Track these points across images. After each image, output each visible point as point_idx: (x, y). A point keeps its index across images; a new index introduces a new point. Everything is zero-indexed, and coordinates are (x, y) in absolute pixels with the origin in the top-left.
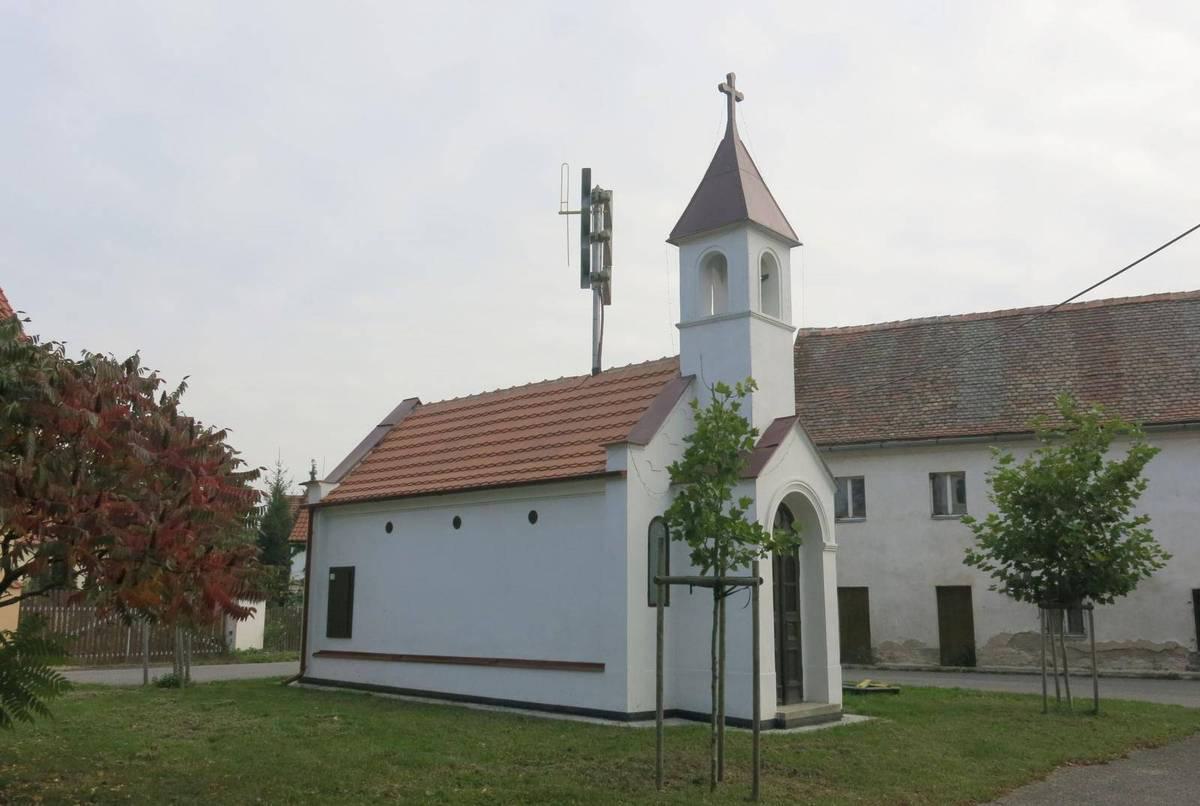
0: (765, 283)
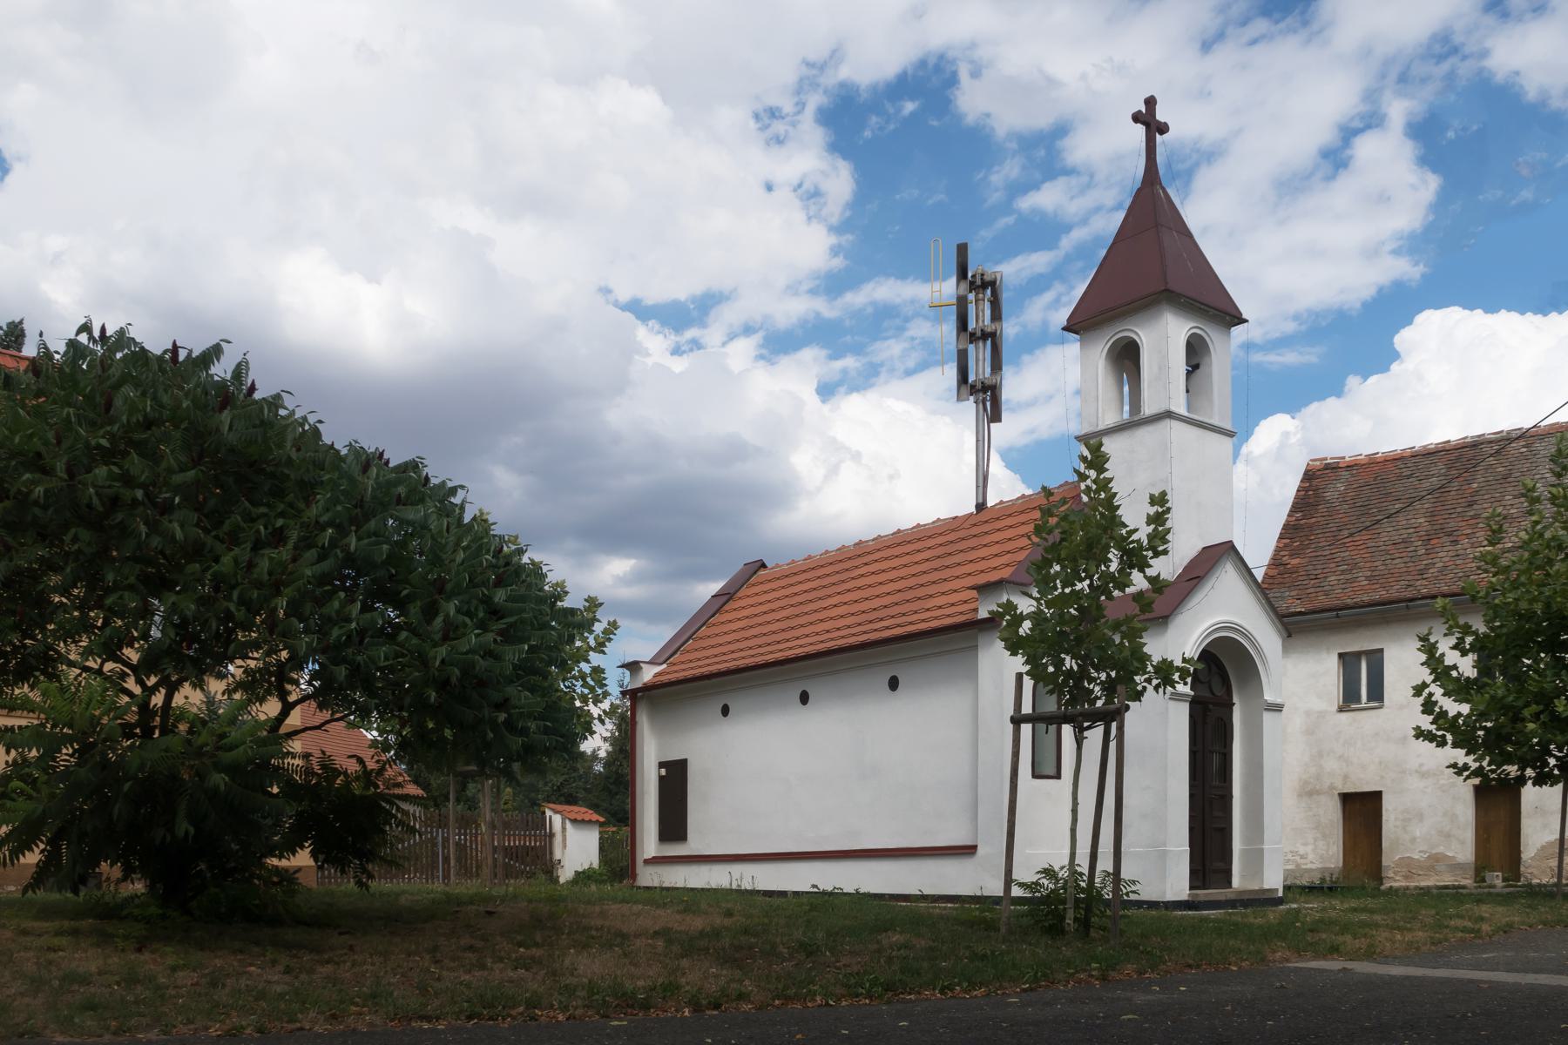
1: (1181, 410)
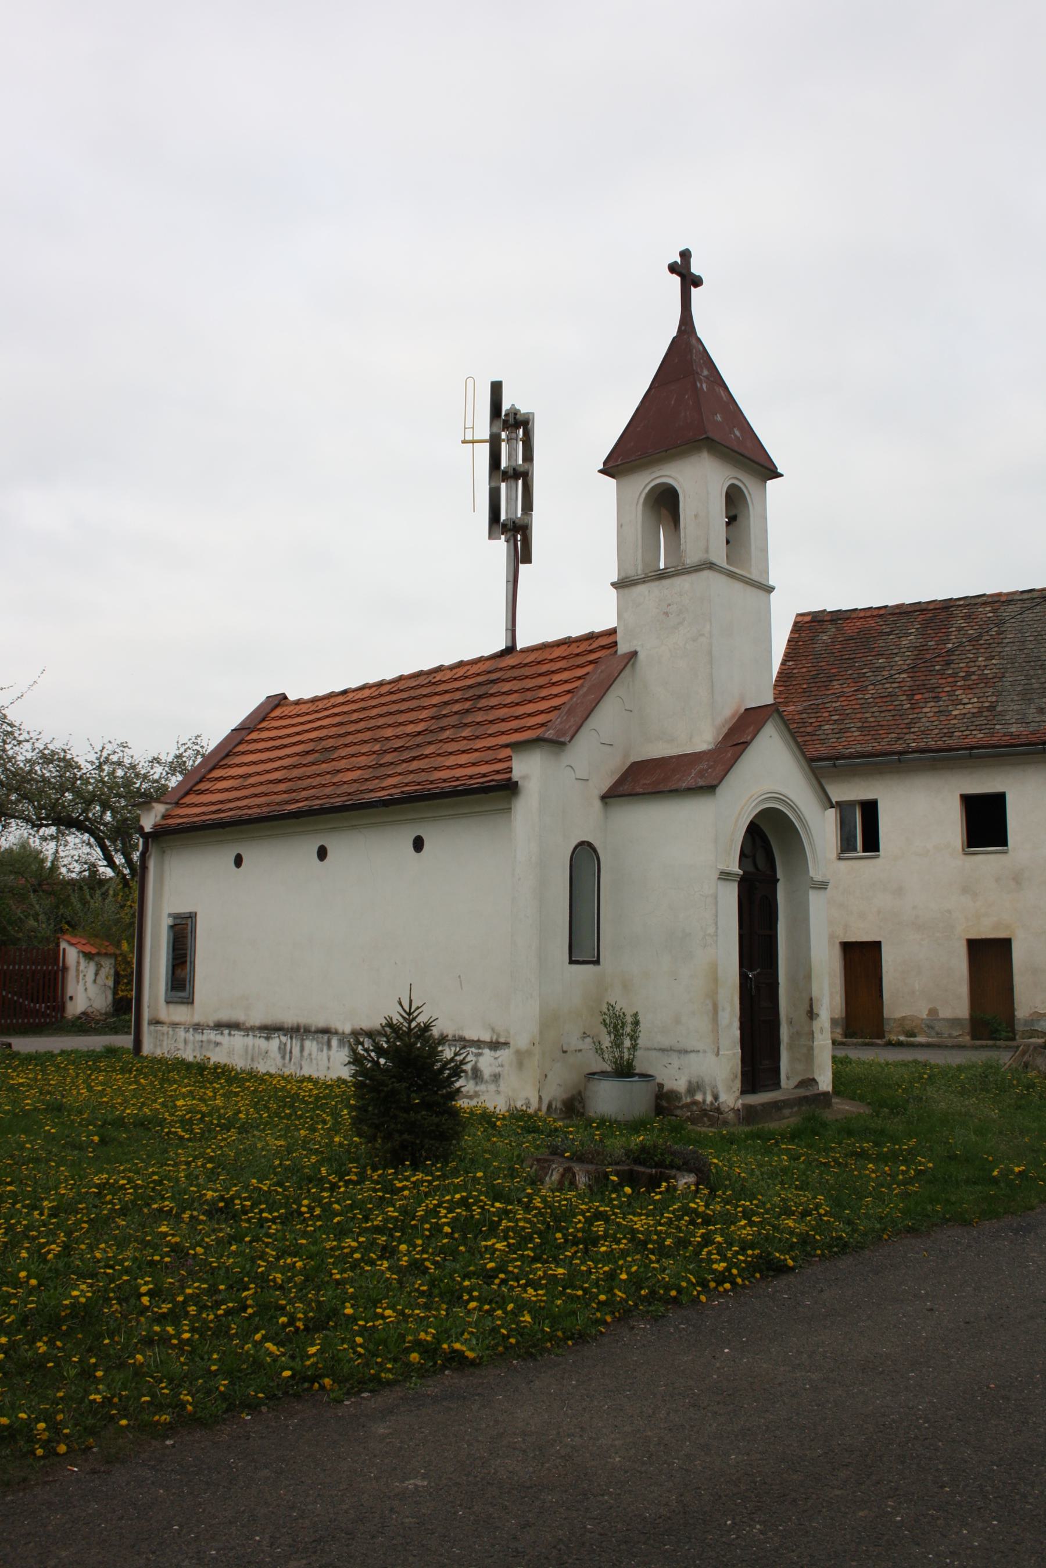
0: (731, 527)
1: (721, 560)
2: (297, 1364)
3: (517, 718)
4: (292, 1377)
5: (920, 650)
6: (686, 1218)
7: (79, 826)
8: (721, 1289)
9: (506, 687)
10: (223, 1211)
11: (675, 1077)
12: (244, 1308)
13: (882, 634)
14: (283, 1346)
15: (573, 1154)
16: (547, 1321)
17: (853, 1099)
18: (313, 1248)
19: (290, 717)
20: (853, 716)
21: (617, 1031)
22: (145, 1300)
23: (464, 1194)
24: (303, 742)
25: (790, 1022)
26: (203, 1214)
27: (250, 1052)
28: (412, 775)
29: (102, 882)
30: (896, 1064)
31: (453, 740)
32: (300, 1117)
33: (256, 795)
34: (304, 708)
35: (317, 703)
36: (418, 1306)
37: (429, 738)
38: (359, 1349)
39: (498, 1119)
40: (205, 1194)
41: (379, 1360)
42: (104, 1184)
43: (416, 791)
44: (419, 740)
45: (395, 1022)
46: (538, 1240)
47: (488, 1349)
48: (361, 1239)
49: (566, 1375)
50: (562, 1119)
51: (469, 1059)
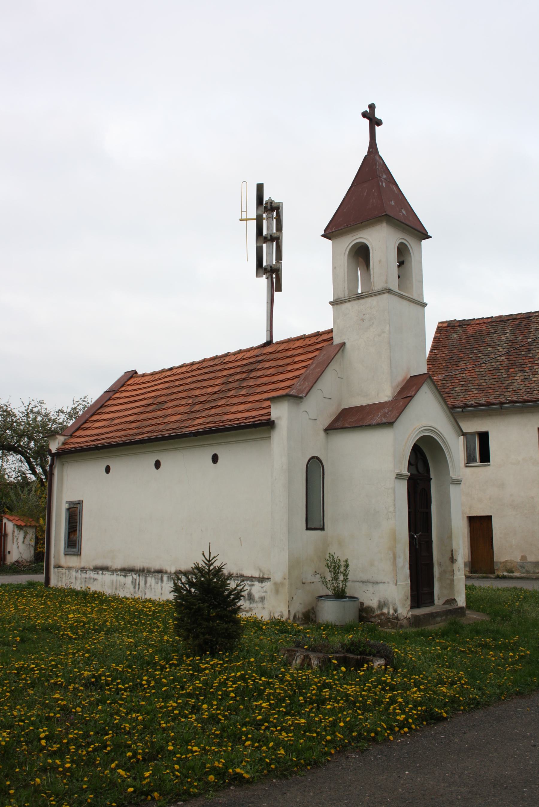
0: (400, 268)
1: (395, 288)
2: (137, 783)
3: (273, 383)
4: (134, 792)
5: (513, 342)
6: (380, 687)
7: (16, 450)
8: (402, 732)
9: (267, 365)
10: (95, 684)
11: (370, 599)
12: (105, 747)
13: (489, 333)
14: (129, 772)
15: (310, 647)
16: (294, 754)
17: (478, 611)
18: (149, 708)
19: (139, 384)
20: (473, 382)
21: (336, 571)
22: (43, 742)
23: (243, 672)
24: (146, 399)
25: (440, 565)
26: (82, 686)
27: (115, 584)
28: (211, 418)
29: (28, 483)
30: (504, 590)
31: (235, 396)
32: (144, 624)
33: (118, 430)
34: (147, 379)
35: (154, 376)
36: (214, 744)
37: (221, 395)
38: (177, 773)
39: (264, 625)
40: (83, 674)
41: (189, 780)
42: (21, 668)
43: (213, 427)
44: (215, 396)
45: (200, 566)
46: (288, 701)
47: (257, 772)
48: (179, 701)
49: (307, 789)
50: (303, 624)
51: (246, 588)
